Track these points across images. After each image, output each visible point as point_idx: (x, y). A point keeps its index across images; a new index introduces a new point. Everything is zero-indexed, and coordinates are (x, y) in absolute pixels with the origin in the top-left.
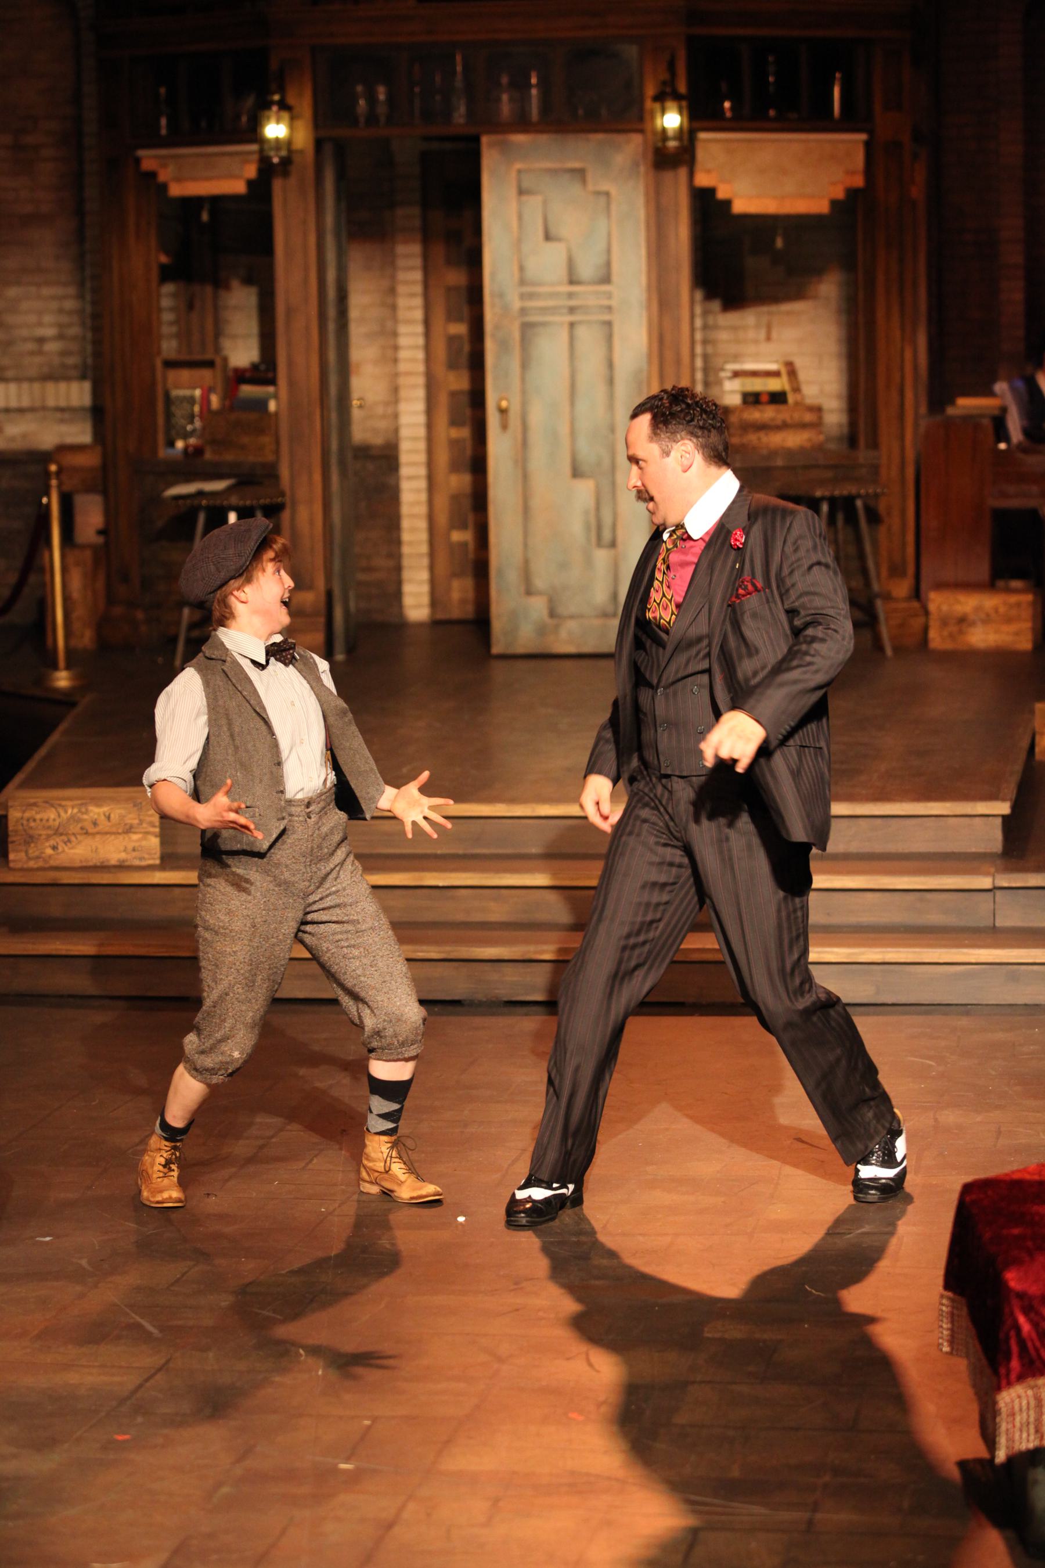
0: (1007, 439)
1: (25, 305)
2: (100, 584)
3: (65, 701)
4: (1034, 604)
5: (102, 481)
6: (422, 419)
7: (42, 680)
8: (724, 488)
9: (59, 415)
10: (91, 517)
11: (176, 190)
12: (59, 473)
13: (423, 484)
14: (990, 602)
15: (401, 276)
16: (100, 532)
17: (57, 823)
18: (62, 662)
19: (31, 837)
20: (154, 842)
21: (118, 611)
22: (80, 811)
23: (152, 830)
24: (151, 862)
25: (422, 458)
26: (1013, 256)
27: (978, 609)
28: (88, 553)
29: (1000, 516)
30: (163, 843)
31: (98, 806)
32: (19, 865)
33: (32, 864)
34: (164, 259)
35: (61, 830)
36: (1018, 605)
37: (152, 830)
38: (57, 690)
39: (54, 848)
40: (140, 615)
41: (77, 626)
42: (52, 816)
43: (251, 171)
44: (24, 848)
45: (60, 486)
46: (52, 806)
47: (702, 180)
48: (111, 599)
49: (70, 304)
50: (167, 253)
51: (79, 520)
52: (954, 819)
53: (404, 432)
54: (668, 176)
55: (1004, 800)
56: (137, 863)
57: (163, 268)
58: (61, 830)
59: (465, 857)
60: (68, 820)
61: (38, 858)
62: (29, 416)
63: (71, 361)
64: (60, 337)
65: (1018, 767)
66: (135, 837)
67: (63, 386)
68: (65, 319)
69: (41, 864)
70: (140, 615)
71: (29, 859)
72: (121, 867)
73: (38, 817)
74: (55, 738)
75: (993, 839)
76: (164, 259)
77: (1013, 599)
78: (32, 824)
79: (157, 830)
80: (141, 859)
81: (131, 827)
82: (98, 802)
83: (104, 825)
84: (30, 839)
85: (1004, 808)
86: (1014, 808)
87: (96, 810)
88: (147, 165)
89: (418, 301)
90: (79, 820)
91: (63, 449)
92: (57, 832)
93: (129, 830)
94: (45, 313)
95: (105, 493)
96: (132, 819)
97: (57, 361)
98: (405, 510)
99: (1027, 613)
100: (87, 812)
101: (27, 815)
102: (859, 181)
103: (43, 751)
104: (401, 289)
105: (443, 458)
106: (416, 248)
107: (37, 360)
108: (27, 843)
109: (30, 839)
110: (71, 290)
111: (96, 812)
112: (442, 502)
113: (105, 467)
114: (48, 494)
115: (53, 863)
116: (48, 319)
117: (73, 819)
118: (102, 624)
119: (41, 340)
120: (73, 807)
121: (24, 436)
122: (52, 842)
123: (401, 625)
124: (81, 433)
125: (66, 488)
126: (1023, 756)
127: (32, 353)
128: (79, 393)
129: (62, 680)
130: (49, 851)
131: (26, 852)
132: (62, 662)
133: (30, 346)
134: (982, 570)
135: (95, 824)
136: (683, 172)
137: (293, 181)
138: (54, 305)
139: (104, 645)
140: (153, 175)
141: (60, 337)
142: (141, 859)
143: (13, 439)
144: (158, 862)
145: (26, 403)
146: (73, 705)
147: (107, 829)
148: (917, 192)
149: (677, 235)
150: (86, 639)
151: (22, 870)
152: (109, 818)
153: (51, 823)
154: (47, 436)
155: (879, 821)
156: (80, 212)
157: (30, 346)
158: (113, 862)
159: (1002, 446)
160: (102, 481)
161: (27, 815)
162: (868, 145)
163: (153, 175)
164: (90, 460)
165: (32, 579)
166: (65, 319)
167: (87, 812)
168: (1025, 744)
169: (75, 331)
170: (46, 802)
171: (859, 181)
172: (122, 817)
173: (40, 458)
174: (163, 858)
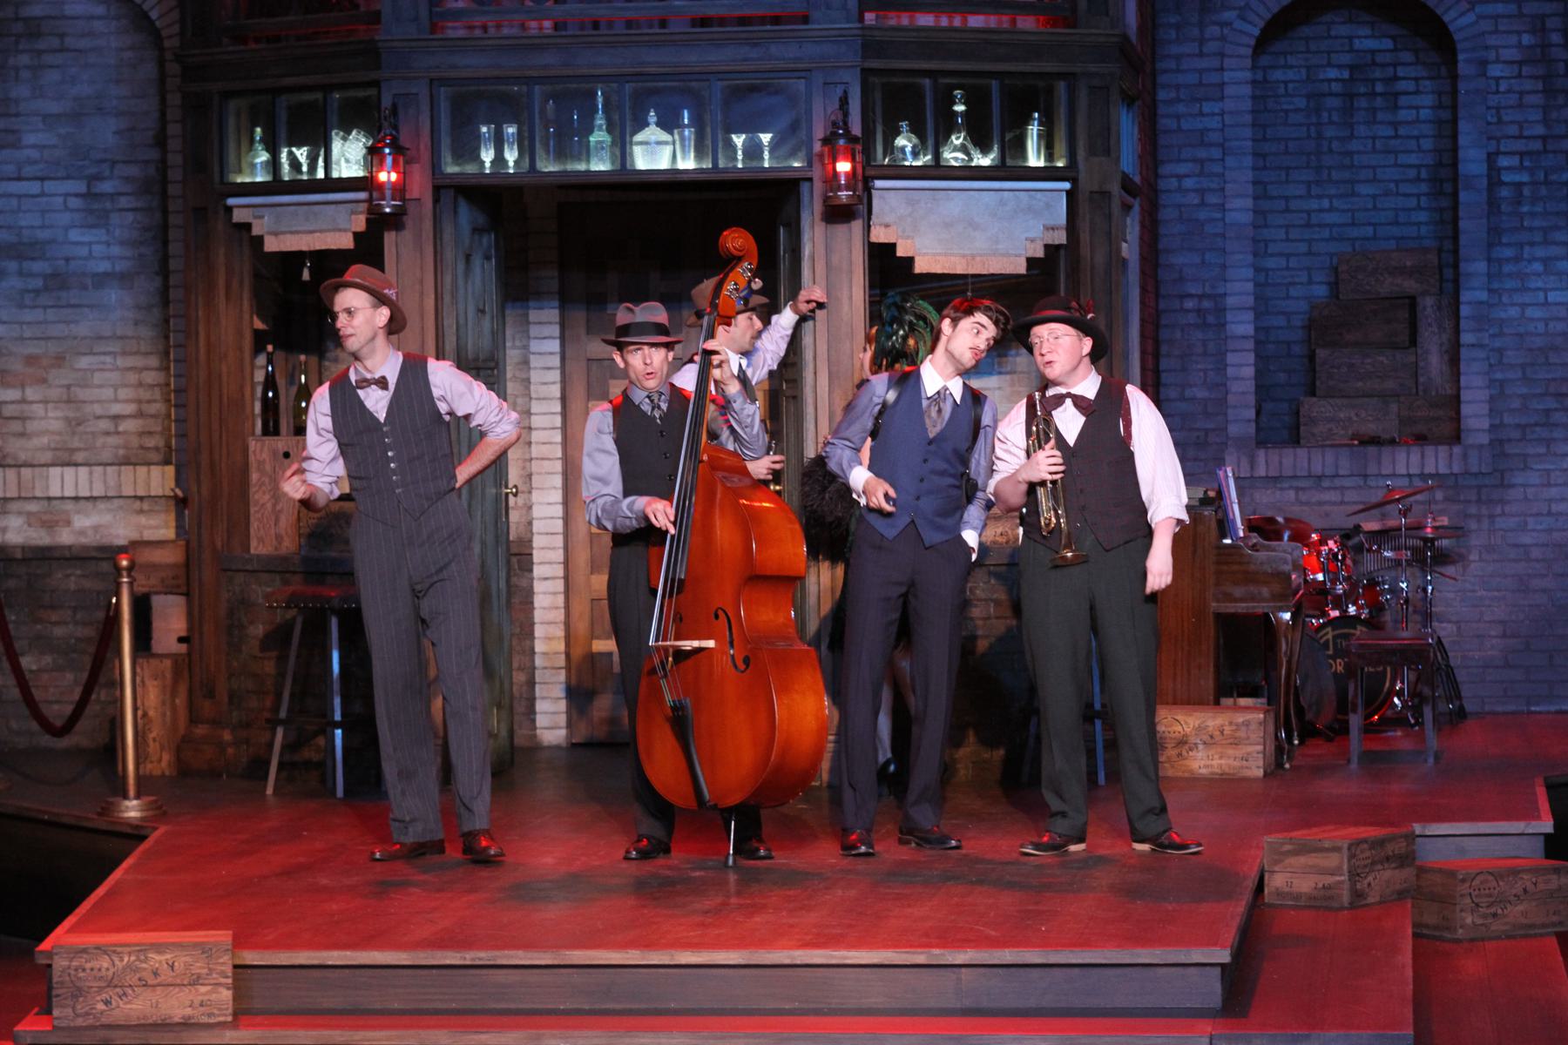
0: (1234, 535)
1: (98, 378)
2: (180, 701)
3: (134, 835)
4: (1264, 723)
5: (185, 581)
6: (558, 511)
7: (107, 810)
8: (1516, 835)
9: (137, 504)
10: (171, 621)
11: (271, 245)
12: (130, 569)
13: (559, 585)
14: (1213, 720)
15: (535, 346)
16: (181, 640)
17: (110, 973)
18: (132, 793)
19: (79, 989)
20: (226, 995)
21: (200, 730)
22: (138, 959)
23: (223, 980)
24: (222, 1019)
25: (559, 555)
26: (1242, 326)
27: (1199, 729)
28: (168, 663)
29: (1224, 620)
30: (235, 999)
31: (159, 953)
32: (64, 1024)
33: (80, 1022)
34: (259, 325)
35: (115, 982)
36: (1247, 724)
37: (223, 980)
38: (128, 823)
39: (107, 1003)
40: (227, 736)
41: (153, 747)
42: (105, 965)
43: (360, 223)
44: (69, 1002)
45: (131, 584)
46: (105, 952)
47: (879, 235)
48: (193, 719)
49: (151, 377)
50: (263, 319)
51: (158, 624)
52: (1165, 970)
53: (537, 526)
54: (840, 230)
55: (1223, 947)
56: (205, 1020)
57: (257, 334)
58: (115, 982)
59: (578, 1012)
60: (124, 968)
61: (87, 1014)
62: (101, 505)
63: (151, 442)
64: (140, 414)
65: (1239, 908)
66: (203, 989)
67: (142, 471)
68: (145, 394)
69: (90, 1021)
70: (227, 736)
71: (78, 1016)
72: (186, 1025)
73: (88, 966)
74: (117, 874)
75: (1211, 990)
76: (259, 325)
77: (1240, 718)
78: (81, 974)
79: (230, 981)
80: (210, 1015)
81: (199, 977)
82: (159, 948)
83: (167, 974)
84: (78, 992)
85: (1224, 956)
86: (1236, 955)
87: (158, 957)
88: (239, 216)
89: (556, 375)
90: (137, 970)
91: (135, 545)
92: (110, 984)
93: (196, 981)
94: (111, 381)
95: (187, 595)
96: (199, 967)
97: (135, 442)
98: (538, 615)
99: (1256, 734)
100: (146, 960)
101: (74, 964)
102: (1061, 238)
103: (101, 891)
104: (535, 361)
105: (582, 557)
106: (552, 314)
107: (112, 440)
108: (75, 997)
109: (78, 992)
110: (154, 361)
111: (156, 959)
112: (581, 607)
113: (187, 564)
114: (118, 595)
115: (104, 1020)
116: (123, 393)
117: (129, 967)
118: (182, 746)
119: (116, 418)
120: (130, 954)
121: (96, 528)
122: (104, 996)
123: (535, 748)
124: (161, 527)
125: (140, 590)
126: (1246, 897)
127: (108, 434)
128: (160, 480)
129: (132, 810)
130: (101, 1006)
131: (74, 1008)
132: (132, 793)
133: (104, 425)
134: (1208, 684)
135: (156, 974)
136: (857, 225)
137: (407, 234)
138: (132, 378)
139: (183, 771)
140: (247, 227)
141: (140, 414)
142: (210, 1015)
143: (82, 532)
144: (230, 1019)
145: (98, 491)
146: (143, 838)
147: (170, 980)
148: (1129, 249)
149: (851, 297)
150: (162, 763)
151: (69, 1028)
152: (172, 967)
153: (104, 972)
154: (119, 527)
155: (1076, 971)
156: (164, 272)
157: (104, 425)
158: (177, 1020)
159: (1228, 541)
160: (185, 581)
161: (74, 964)
162: (1070, 194)
163: (247, 227)
164: (171, 556)
165: (100, 694)
166: (145, 394)
167: (146, 960)
168: (1251, 883)
169: (158, 407)
170: (98, 948)
171: (1061, 238)
172: (188, 966)
173: (109, 553)
174: (235, 1014)
